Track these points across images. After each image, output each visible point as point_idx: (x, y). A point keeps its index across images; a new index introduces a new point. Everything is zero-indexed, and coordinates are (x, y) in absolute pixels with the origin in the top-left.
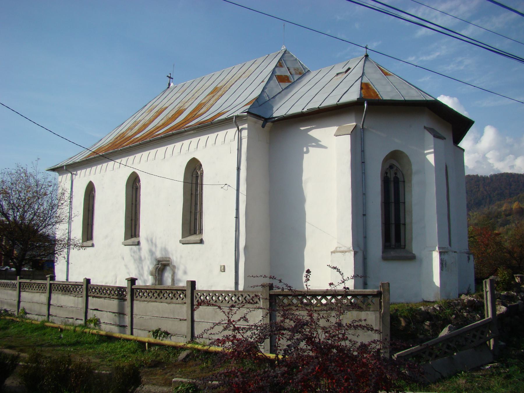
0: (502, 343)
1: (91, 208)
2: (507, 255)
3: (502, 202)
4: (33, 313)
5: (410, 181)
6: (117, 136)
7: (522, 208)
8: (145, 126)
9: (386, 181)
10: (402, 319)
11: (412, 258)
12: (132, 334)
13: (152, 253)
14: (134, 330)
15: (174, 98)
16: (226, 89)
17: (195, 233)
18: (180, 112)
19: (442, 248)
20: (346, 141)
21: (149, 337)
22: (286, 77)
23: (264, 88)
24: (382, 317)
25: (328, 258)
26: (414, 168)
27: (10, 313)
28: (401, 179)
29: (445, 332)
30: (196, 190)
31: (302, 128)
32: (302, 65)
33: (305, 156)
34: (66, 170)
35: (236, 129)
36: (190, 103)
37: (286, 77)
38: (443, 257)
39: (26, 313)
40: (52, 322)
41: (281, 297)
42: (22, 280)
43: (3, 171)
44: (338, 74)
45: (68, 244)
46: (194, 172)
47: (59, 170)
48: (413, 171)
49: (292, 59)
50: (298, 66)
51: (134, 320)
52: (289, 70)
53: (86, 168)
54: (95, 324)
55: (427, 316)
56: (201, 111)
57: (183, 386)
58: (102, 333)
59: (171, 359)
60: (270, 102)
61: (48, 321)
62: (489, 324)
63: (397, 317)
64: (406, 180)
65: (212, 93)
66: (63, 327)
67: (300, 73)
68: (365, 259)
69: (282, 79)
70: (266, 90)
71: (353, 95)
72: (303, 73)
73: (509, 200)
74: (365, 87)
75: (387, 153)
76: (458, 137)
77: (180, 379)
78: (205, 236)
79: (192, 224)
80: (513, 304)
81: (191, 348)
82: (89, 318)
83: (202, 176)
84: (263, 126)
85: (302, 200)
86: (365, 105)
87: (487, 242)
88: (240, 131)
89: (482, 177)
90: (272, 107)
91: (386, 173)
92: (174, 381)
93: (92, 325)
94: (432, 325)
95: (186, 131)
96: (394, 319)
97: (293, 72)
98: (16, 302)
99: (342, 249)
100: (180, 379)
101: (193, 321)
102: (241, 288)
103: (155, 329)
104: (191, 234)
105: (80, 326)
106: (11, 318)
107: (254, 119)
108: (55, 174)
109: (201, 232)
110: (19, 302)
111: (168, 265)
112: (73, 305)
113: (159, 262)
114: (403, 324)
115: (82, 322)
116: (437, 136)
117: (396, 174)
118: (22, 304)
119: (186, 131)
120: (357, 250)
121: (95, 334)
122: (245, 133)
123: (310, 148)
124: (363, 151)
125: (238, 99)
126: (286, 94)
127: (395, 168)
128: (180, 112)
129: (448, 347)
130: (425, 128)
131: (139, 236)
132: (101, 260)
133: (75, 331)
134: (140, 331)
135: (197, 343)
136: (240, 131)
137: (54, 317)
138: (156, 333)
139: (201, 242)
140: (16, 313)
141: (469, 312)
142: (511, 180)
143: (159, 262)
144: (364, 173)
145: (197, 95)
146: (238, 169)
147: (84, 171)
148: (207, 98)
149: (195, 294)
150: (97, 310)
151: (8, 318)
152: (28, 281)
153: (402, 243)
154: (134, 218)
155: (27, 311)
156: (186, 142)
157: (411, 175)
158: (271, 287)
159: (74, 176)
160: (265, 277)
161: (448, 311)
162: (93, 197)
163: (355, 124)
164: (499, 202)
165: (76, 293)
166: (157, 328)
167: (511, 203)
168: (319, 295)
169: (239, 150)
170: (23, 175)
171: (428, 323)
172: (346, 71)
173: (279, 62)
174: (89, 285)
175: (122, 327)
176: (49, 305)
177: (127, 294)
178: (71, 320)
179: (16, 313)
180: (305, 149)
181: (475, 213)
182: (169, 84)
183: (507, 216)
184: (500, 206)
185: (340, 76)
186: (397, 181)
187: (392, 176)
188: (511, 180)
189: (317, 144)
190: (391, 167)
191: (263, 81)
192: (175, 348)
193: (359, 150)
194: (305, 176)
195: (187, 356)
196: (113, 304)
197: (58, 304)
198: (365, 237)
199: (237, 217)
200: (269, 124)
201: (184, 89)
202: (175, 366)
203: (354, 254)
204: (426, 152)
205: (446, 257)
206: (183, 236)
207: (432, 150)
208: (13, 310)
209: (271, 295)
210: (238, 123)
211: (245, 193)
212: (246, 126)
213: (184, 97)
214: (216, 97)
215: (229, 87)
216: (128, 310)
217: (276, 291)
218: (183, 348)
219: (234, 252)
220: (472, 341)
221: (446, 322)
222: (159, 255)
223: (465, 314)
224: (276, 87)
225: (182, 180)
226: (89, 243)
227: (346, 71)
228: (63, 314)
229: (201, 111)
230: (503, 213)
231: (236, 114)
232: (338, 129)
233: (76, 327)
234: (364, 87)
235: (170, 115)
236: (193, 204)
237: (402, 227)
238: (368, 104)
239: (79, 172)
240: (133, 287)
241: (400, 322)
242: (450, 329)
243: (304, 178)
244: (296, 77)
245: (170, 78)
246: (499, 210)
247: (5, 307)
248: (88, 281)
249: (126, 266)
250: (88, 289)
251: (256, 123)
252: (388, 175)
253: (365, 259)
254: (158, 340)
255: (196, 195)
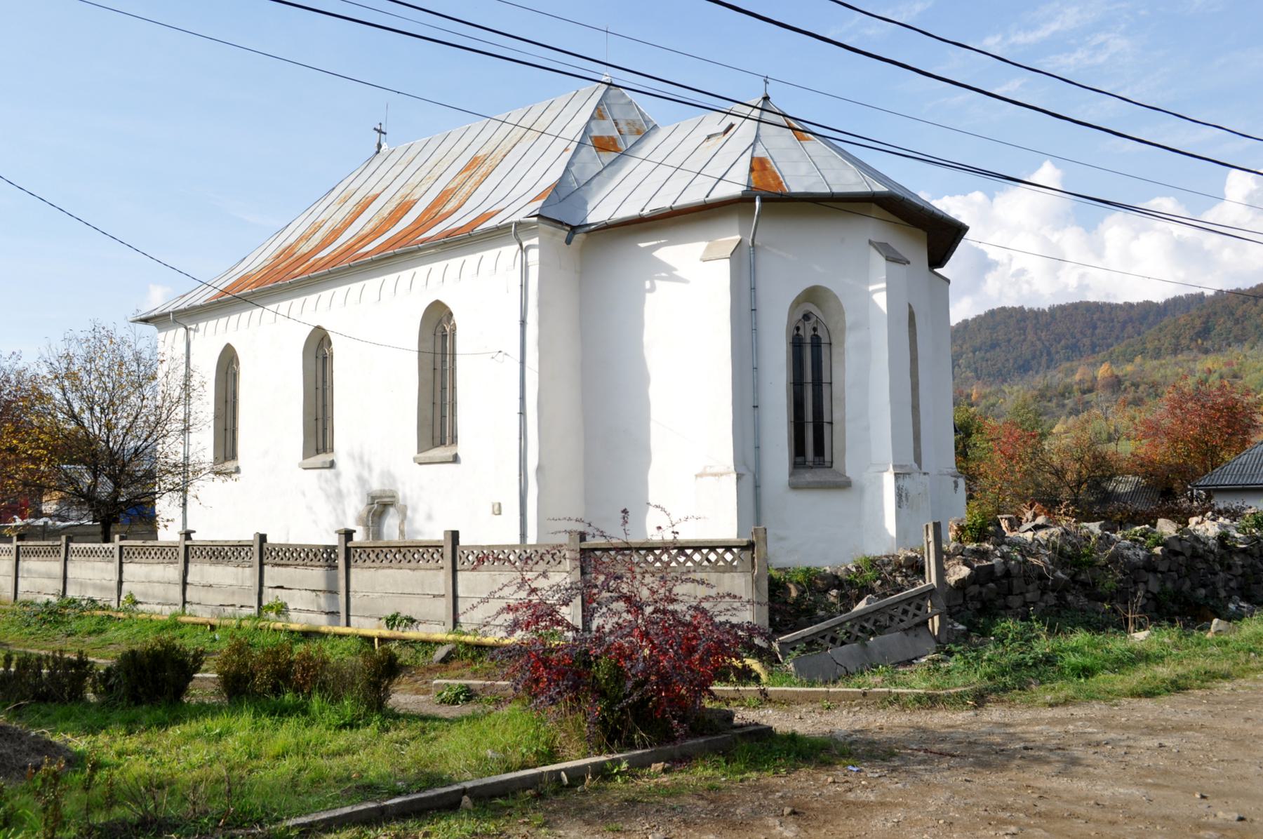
0: (961, 627)
1: (230, 396)
2: (1054, 479)
3: (1075, 363)
4: (151, 601)
5: (843, 342)
6: (278, 252)
7: (1117, 377)
8: (336, 233)
9: (796, 344)
10: (791, 586)
11: (844, 484)
12: (348, 624)
13: (361, 480)
14: (352, 618)
15: (391, 176)
16: (494, 162)
17: (443, 443)
18: (404, 208)
19: (901, 467)
20: (721, 271)
21: (379, 627)
22: (608, 144)
23: (570, 164)
24: (756, 582)
25: (691, 486)
26: (849, 318)
27: (101, 604)
28: (825, 340)
29: (862, 605)
30: (444, 362)
31: (642, 245)
32: (642, 114)
33: (648, 296)
34: (175, 321)
35: (518, 246)
36: (424, 188)
37: (608, 144)
38: (901, 482)
39: (136, 603)
40: (190, 615)
41: (598, 553)
42: (123, 543)
43: (67, 336)
44: (709, 137)
45: (186, 470)
46: (438, 327)
47: (159, 320)
48: (848, 324)
49: (623, 101)
50: (634, 116)
51: (352, 600)
52: (617, 124)
53: (217, 317)
54: (278, 613)
55: (835, 581)
56: (449, 207)
57: (451, 690)
58: (295, 627)
59: (421, 661)
60: (581, 193)
61: (184, 613)
62: (930, 593)
63: (784, 583)
64: (833, 341)
65: (466, 168)
66: (216, 622)
67: (638, 132)
68: (757, 486)
69: (604, 145)
70: (573, 169)
71: (733, 188)
72: (644, 131)
73: (1091, 360)
74: (759, 166)
75: (799, 291)
76: (938, 257)
77: (444, 681)
78: (462, 448)
79: (437, 426)
80: (985, 563)
81: (454, 641)
82: (265, 603)
83: (453, 335)
84: (568, 242)
85: (643, 379)
86: (757, 203)
87: (1011, 451)
88: (524, 250)
89: (1031, 310)
90: (586, 203)
91: (798, 329)
92: (436, 685)
93: (272, 615)
94: (842, 597)
95: (420, 249)
96: (776, 588)
97: (625, 129)
98: (114, 584)
99: (715, 470)
100: (444, 681)
101: (455, 597)
102: (532, 539)
103: (389, 615)
104: (434, 446)
105: (249, 617)
106: (107, 613)
107: (551, 229)
108: (150, 329)
109: (454, 440)
110: (120, 582)
111: (392, 504)
112: (234, 582)
113: (373, 498)
114: (794, 593)
115: (254, 611)
116: (893, 258)
117: (815, 329)
118: (125, 586)
119: (420, 249)
120: (742, 471)
121: (280, 631)
122: (534, 255)
123: (658, 283)
124: (753, 289)
125: (517, 190)
126: (611, 177)
127: (813, 320)
128: (404, 208)
129: (863, 629)
130: (870, 242)
131: (332, 451)
132: (252, 499)
133: (239, 627)
134: (362, 620)
135: (464, 634)
136: (524, 250)
137: (195, 607)
138: (392, 621)
139: (455, 459)
140: (114, 604)
141: (906, 576)
142: (1095, 317)
143: (373, 498)
144: (755, 330)
145: (437, 172)
146: (523, 323)
147: (212, 323)
148: (458, 180)
149: (459, 553)
150: (282, 587)
151: (99, 613)
152: (139, 543)
153: (827, 457)
154: (320, 416)
155: (138, 598)
156: (422, 270)
157: (843, 331)
158: (583, 537)
159: (192, 333)
160: (570, 519)
161: (869, 574)
162: (235, 376)
163: (738, 237)
164: (1068, 364)
165: (240, 559)
166: (394, 613)
167: (1094, 365)
168: (658, 548)
169: (524, 287)
170: (106, 342)
171: (834, 592)
172: (726, 132)
173: (597, 108)
174: (265, 546)
175: (333, 614)
176: (185, 584)
177: (340, 557)
178: (230, 609)
179: (114, 604)
180: (648, 285)
181: (1015, 388)
182: (380, 146)
183: (1084, 392)
184: (1072, 371)
185: (713, 140)
186: (816, 343)
187: (807, 334)
188: (1095, 317)
189: (670, 274)
190: (806, 317)
191: (566, 150)
192: (425, 642)
193: (746, 286)
194: (648, 336)
195: (449, 653)
196: (316, 576)
197: (204, 582)
198: (758, 447)
199: (522, 413)
200: (579, 237)
201: (412, 156)
202: (429, 669)
203: (738, 479)
204: (871, 288)
205: (907, 483)
206: (420, 450)
207: (884, 285)
208: (110, 598)
209: (582, 550)
210: (521, 236)
211: (536, 367)
212: (535, 241)
213: (412, 175)
214: (476, 178)
215: (500, 157)
216: (342, 583)
217: (591, 542)
218: (439, 643)
219: (518, 478)
220: (902, 621)
221: (865, 590)
222: (376, 486)
223: (899, 579)
224: (592, 161)
225: (416, 348)
226: (230, 465)
227: (726, 132)
228: (215, 598)
229: (449, 207)
230: (1076, 387)
231: (515, 218)
232: (708, 248)
233: (241, 620)
234: (757, 167)
235: (385, 213)
236: (438, 388)
237: (826, 428)
238: (763, 200)
239: (202, 325)
240: (349, 545)
241: (788, 590)
242: (868, 603)
243: (646, 338)
244: (631, 140)
245: (380, 131)
246: (1068, 380)
247: (90, 594)
248: (263, 538)
249: (310, 508)
250: (263, 552)
251: (554, 234)
252: (801, 332)
253: (757, 486)
254: (396, 633)
255: (443, 371)
